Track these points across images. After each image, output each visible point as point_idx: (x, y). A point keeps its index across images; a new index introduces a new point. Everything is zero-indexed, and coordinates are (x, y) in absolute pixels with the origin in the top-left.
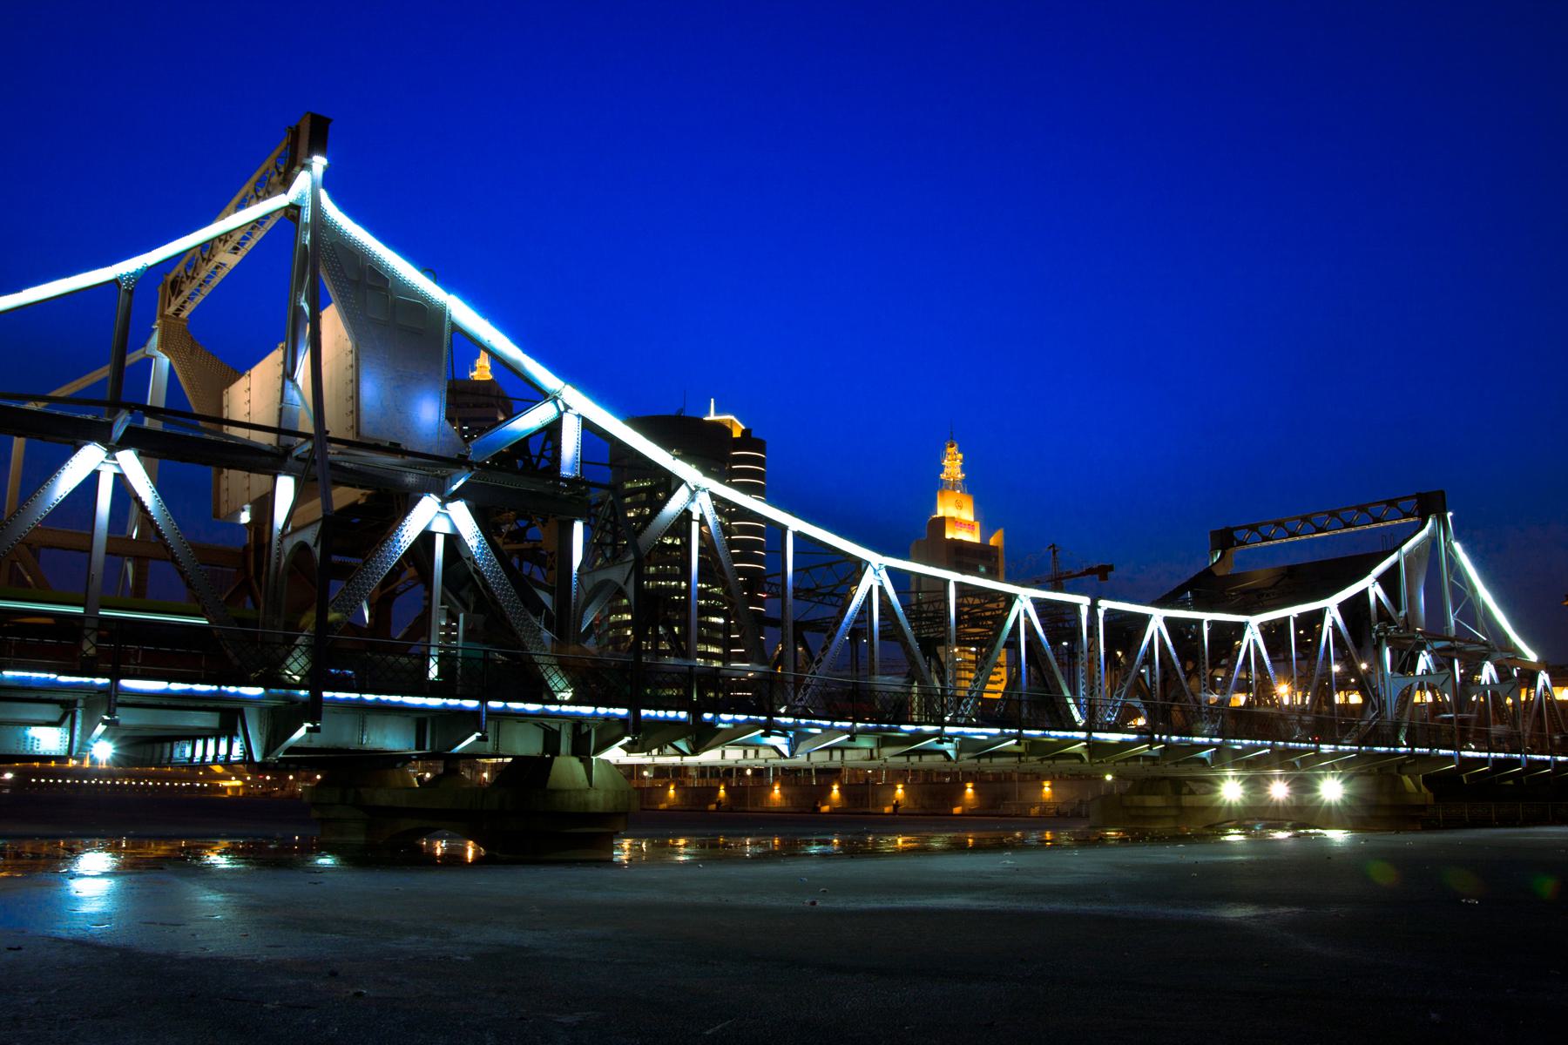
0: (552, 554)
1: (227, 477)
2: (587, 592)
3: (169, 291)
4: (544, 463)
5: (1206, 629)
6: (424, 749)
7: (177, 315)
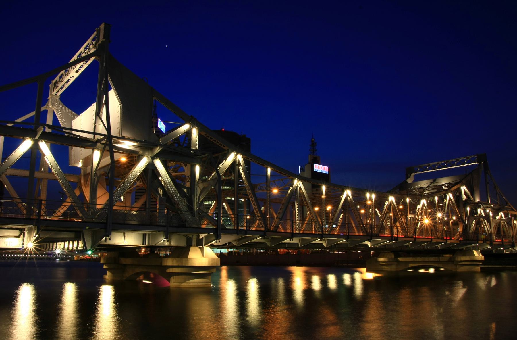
0: (188, 177)
1: (74, 151)
2: (201, 189)
3: (53, 86)
4: (185, 145)
5: (269, 215)
6: (146, 244)
7: (56, 94)
